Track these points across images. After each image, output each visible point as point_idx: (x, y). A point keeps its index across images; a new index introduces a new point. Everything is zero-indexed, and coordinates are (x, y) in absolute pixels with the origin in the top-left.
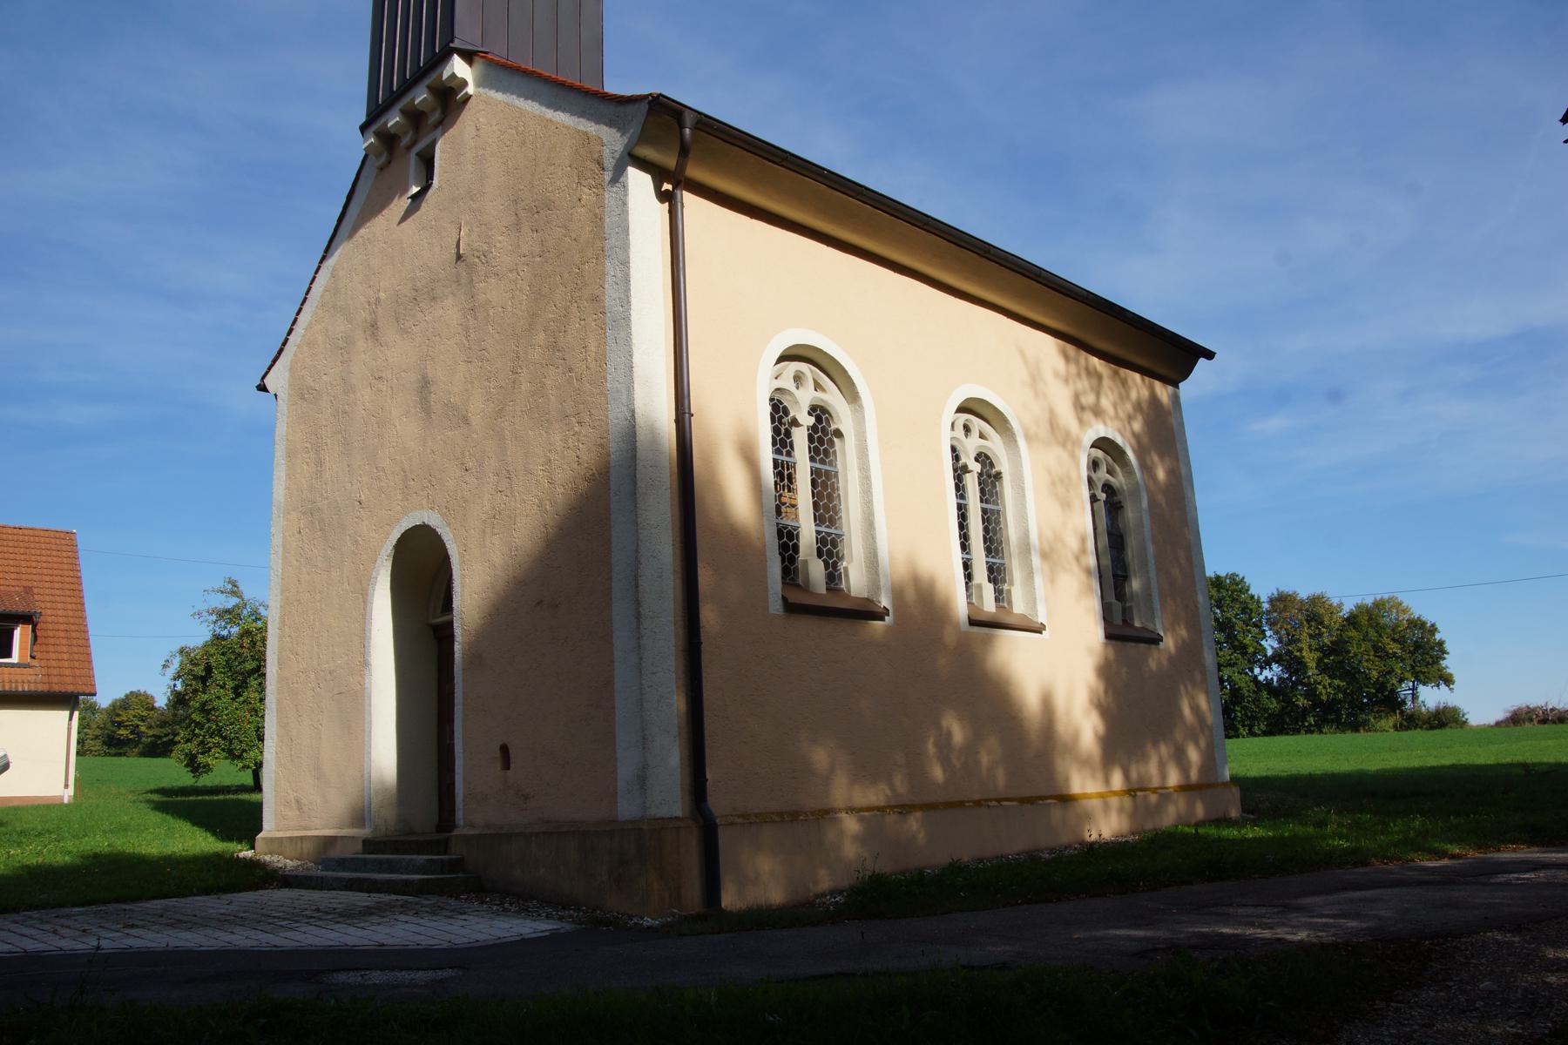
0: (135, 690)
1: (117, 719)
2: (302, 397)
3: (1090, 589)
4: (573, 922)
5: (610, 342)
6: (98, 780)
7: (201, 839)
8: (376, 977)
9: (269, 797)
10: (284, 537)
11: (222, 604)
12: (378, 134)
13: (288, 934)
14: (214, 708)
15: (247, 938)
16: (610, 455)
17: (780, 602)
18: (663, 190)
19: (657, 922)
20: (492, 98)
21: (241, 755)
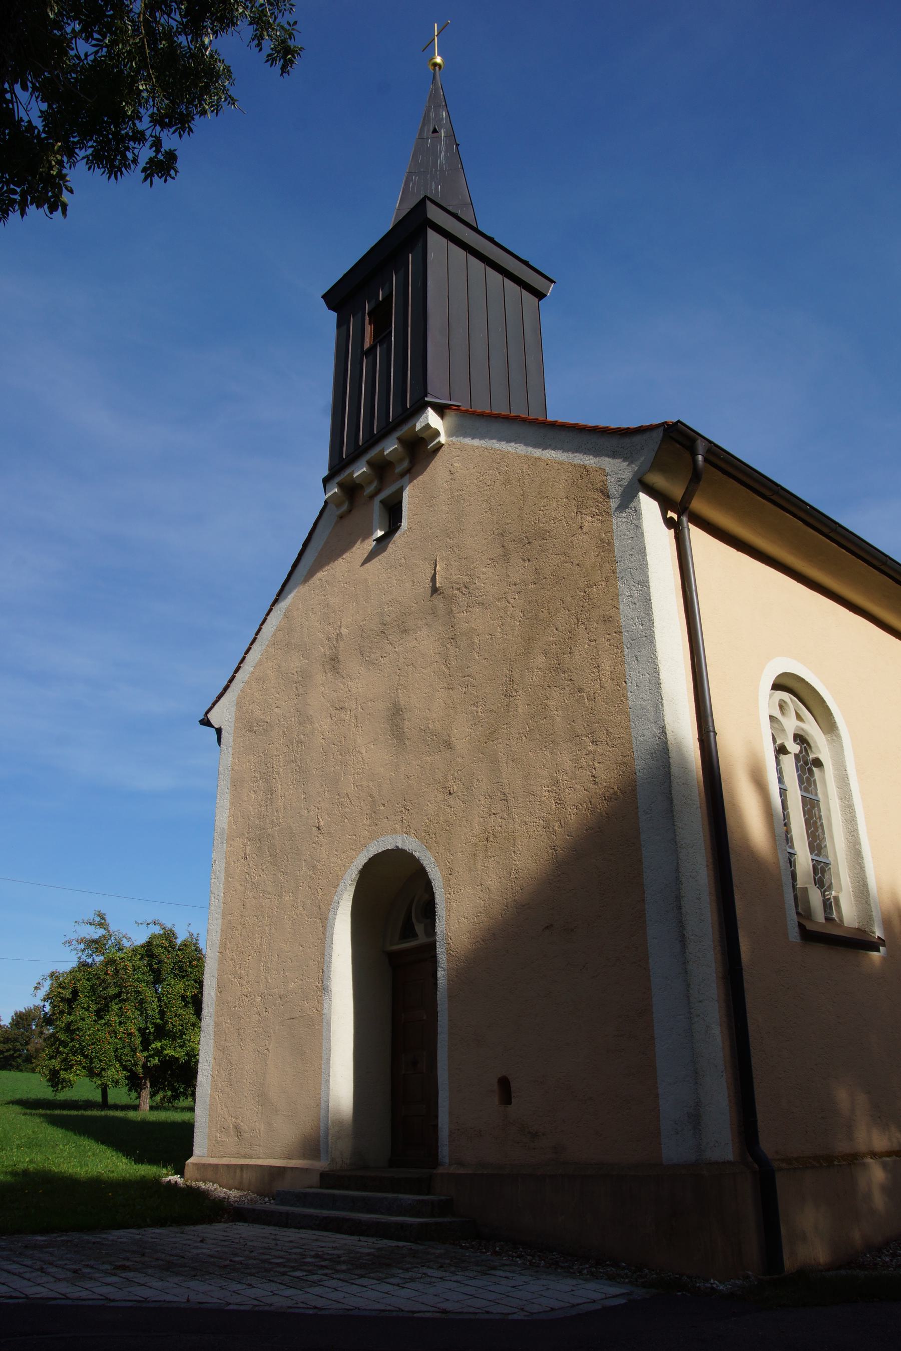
2: (251, 729)
5: (630, 660)
10: (227, 863)
13: (317, 1290)
16: (635, 774)
17: (797, 929)
18: (668, 517)
20: (468, 445)
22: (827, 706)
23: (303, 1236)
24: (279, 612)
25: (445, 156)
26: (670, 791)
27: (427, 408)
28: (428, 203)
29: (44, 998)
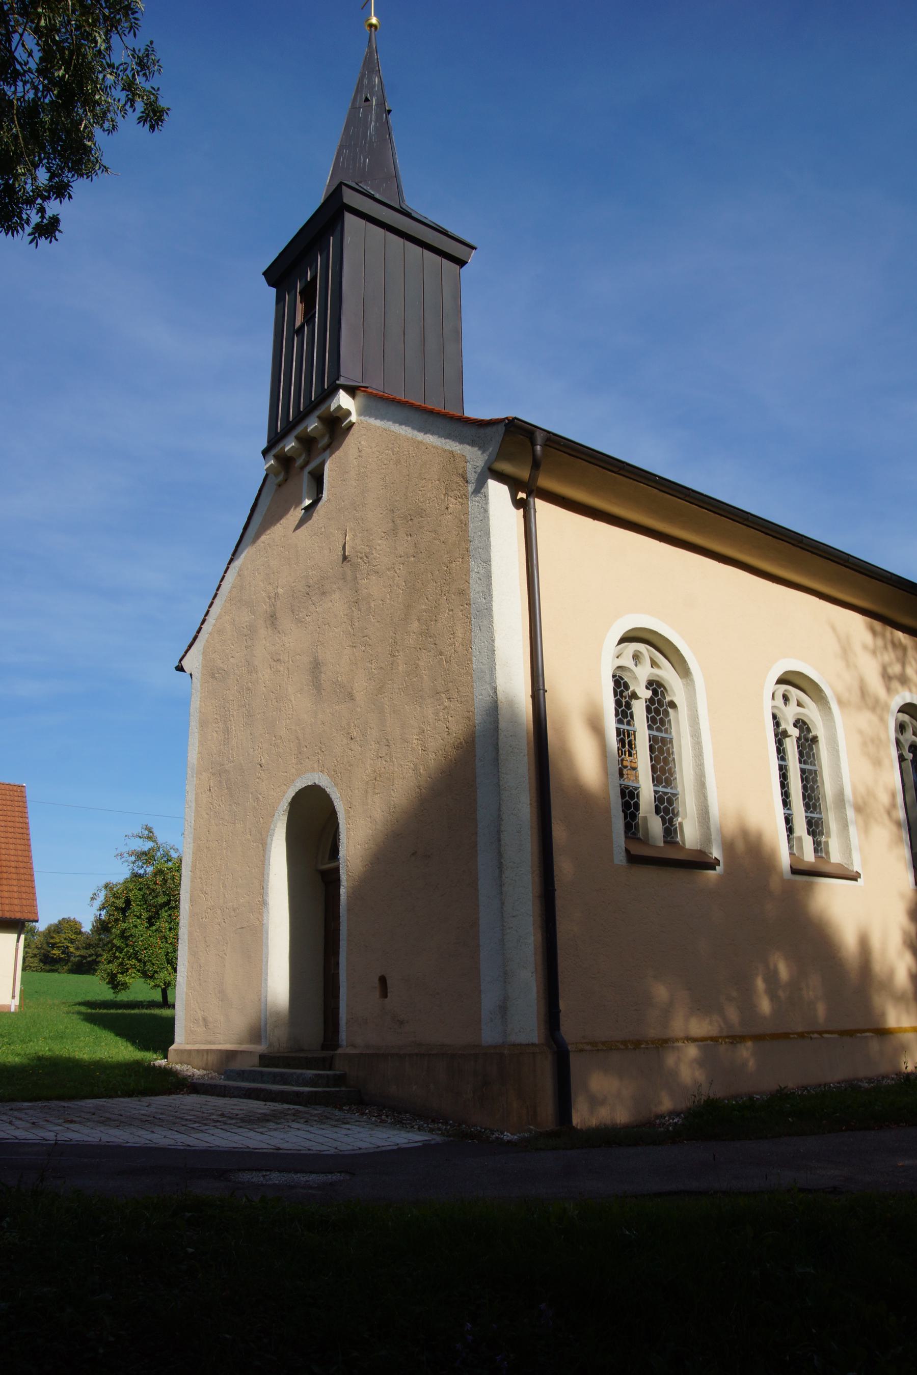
0: (66, 916)
1: (52, 941)
2: (213, 676)
3: (900, 839)
4: (442, 1134)
5: (475, 629)
6: (36, 992)
7: (123, 1048)
8: (276, 1178)
9: (180, 1013)
10: (197, 794)
11: (139, 847)
12: (276, 457)
13: (200, 1135)
14: (131, 935)
15: (165, 1137)
16: (475, 727)
17: (623, 854)
18: (518, 498)
19: (516, 1137)
20: (372, 425)
21: (153, 975)
22: (682, 655)
23: (226, 1102)
24: (234, 570)
25: (375, 126)
26: (497, 743)
27: (339, 390)
28: (344, 188)
29: (100, 907)
